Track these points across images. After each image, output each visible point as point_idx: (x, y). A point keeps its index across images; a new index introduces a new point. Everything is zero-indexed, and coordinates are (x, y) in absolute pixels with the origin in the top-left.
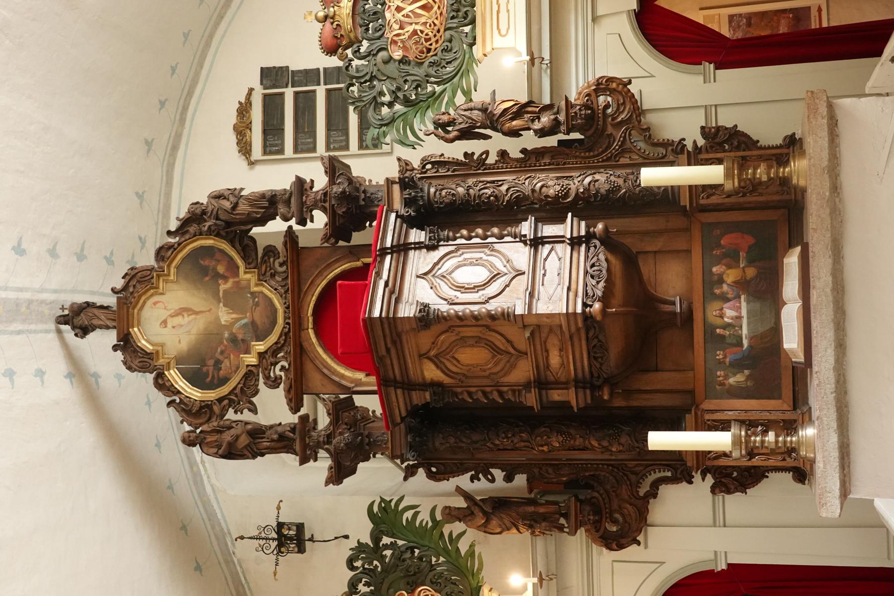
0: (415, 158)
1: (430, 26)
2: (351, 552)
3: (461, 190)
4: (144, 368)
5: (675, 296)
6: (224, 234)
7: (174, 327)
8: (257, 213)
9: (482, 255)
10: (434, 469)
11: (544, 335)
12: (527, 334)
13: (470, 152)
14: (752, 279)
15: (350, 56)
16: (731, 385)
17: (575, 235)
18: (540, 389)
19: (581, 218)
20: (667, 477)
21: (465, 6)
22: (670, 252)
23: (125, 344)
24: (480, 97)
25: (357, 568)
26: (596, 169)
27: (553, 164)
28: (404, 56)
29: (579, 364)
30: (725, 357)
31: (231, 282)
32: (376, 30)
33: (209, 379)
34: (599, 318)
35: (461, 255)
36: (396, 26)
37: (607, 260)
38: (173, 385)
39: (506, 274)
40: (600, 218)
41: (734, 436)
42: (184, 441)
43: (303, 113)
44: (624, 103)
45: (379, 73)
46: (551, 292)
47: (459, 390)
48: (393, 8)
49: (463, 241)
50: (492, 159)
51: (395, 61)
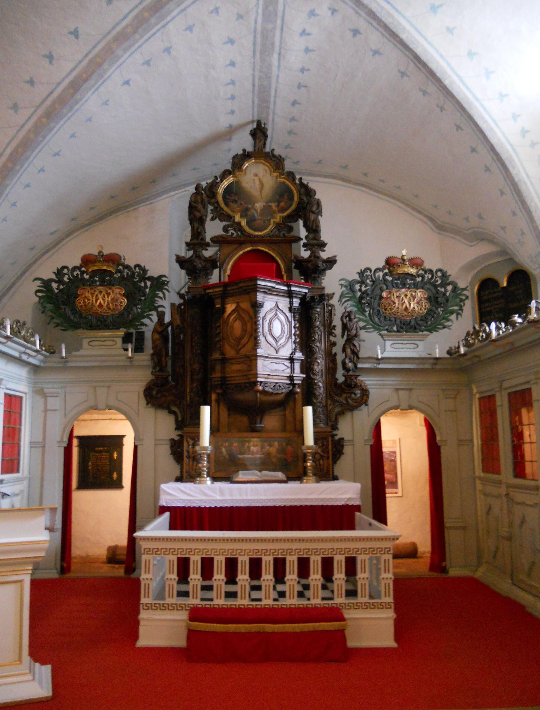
0: (334, 301)
3: (318, 323)
9: (286, 333)
10: (182, 307)
13: (336, 328)
15: (385, 271)
17: (295, 378)
19: (303, 381)
24: (363, 334)
25: (135, 269)
26: (326, 388)
29: (233, 378)
34: (255, 389)
37: (282, 393)
40: (302, 390)
44: (356, 402)
49: (293, 325)
50: (332, 339)
51: (381, 293)
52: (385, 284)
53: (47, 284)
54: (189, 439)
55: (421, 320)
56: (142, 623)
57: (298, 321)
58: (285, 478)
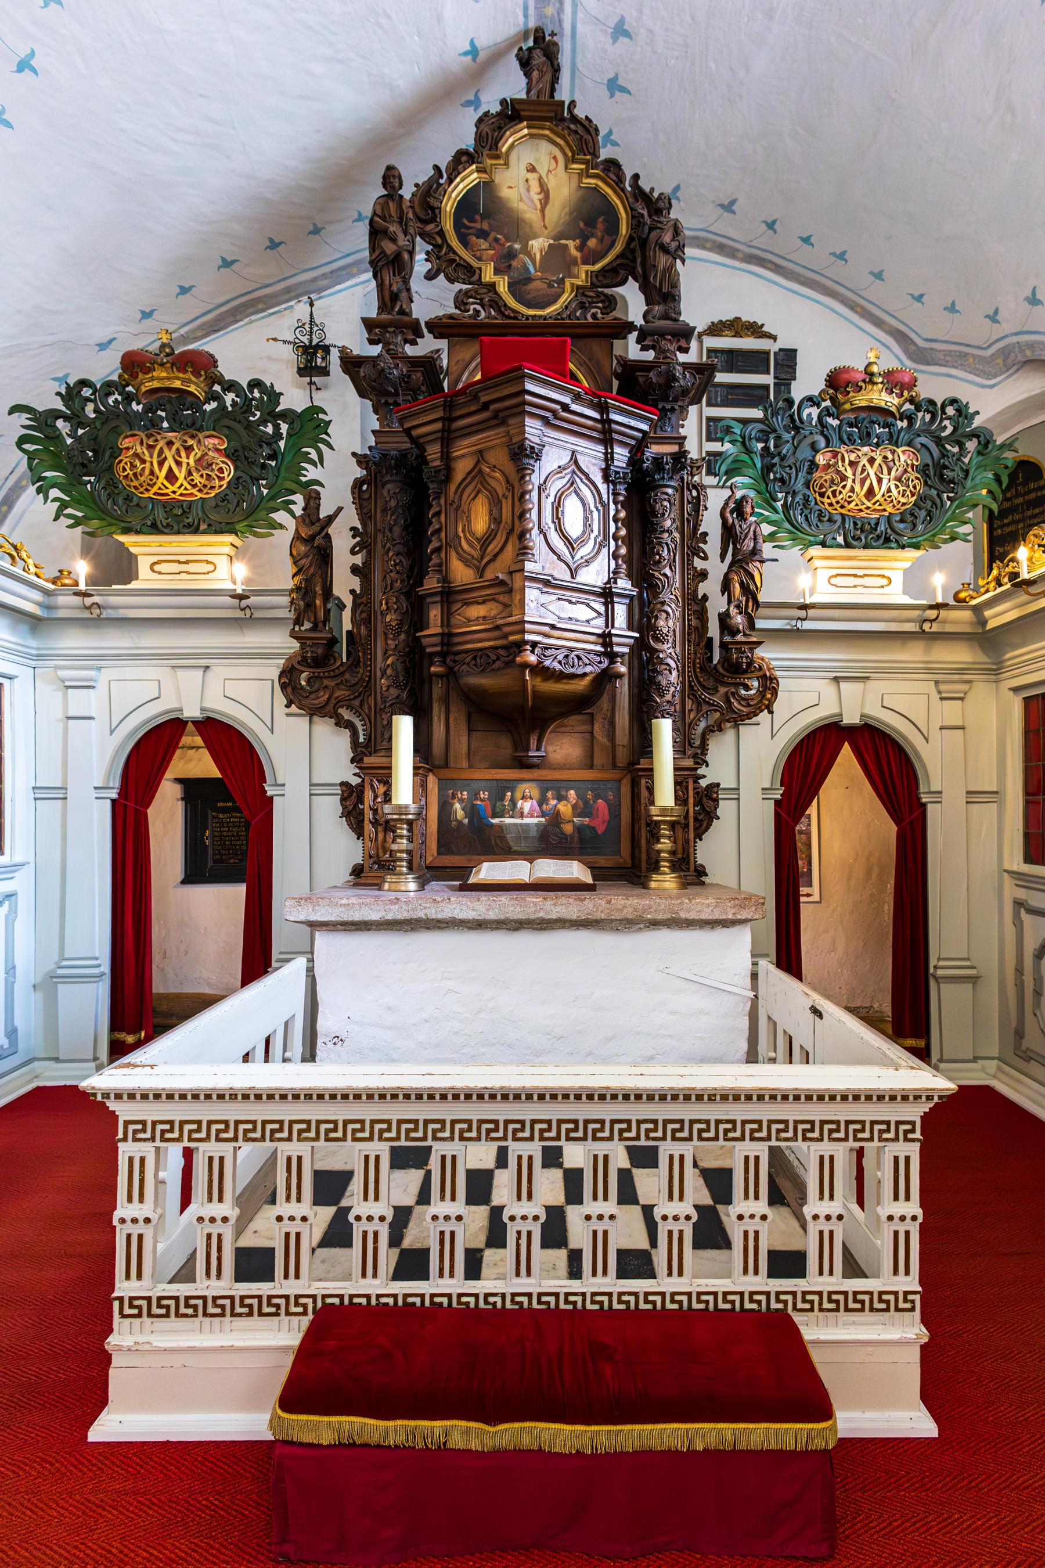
1: (850, 497)
2: (268, 384)
3: (668, 523)
4: (479, 138)
5: (545, 751)
6: (632, 246)
7: (527, 181)
8: (655, 277)
9: (596, 532)
10: (365, 487)
11: (501, 598)
12: (501, 576)
13: (707, 539)
14: (561, 829)
15: (824, 404)
16: (452, 805)
17: (615, 639)
18: (441, 593)
19: (632, 648)
20: (358, 738)
21: (866, 538)
22: (592, 744)
23: (507, 116)
24: (767, 550)
25: (252, 393)
26: (682, 673)
27: (689, 629)
28: (818, 466)
29: (468, 637)
30: (482, 800)
31: (574, 252)
32: (850, 435)
33: (465, 221)
35: (596, 507)
36: (853, 457)
37: (585, 675)
38: (459, 173)
39: (573, 558)
40: (630, 668)
41: (407, 807)
42: (426, 277)
43: (748, 395)
44: (749, 705)
45: (802, 437)
46: (550, 608)
47: (442, 501)
48: (873, 454)
49: (612, 513)
50: (698, 563)
51: (814, 456)
52: (822, 433)
53: (44, 421)
54: (376, 784)
55: (902, 521)
56: (116, 1361)
57: (624, 505)
58: (589, 879)
